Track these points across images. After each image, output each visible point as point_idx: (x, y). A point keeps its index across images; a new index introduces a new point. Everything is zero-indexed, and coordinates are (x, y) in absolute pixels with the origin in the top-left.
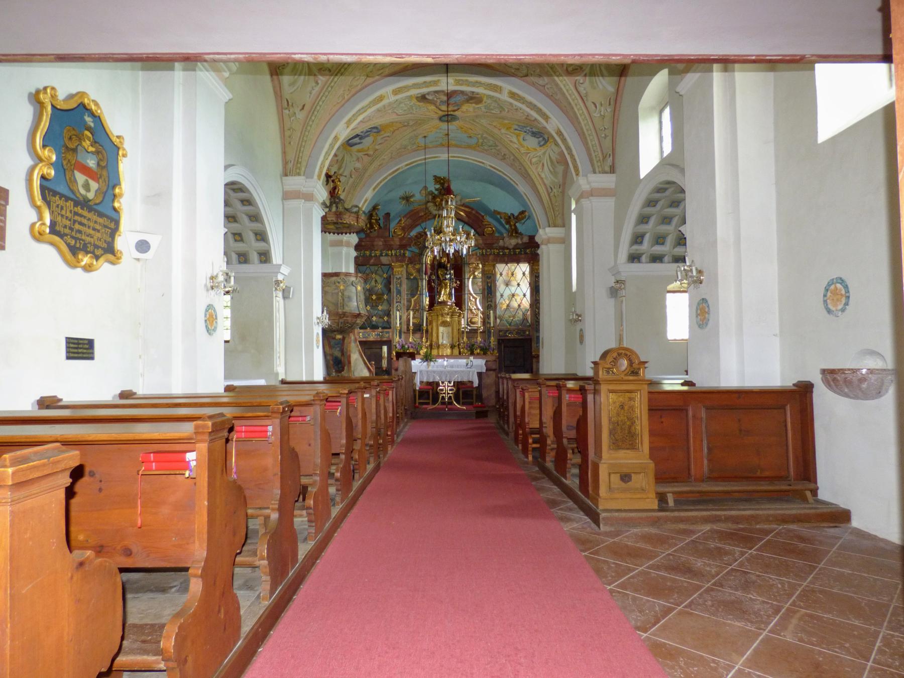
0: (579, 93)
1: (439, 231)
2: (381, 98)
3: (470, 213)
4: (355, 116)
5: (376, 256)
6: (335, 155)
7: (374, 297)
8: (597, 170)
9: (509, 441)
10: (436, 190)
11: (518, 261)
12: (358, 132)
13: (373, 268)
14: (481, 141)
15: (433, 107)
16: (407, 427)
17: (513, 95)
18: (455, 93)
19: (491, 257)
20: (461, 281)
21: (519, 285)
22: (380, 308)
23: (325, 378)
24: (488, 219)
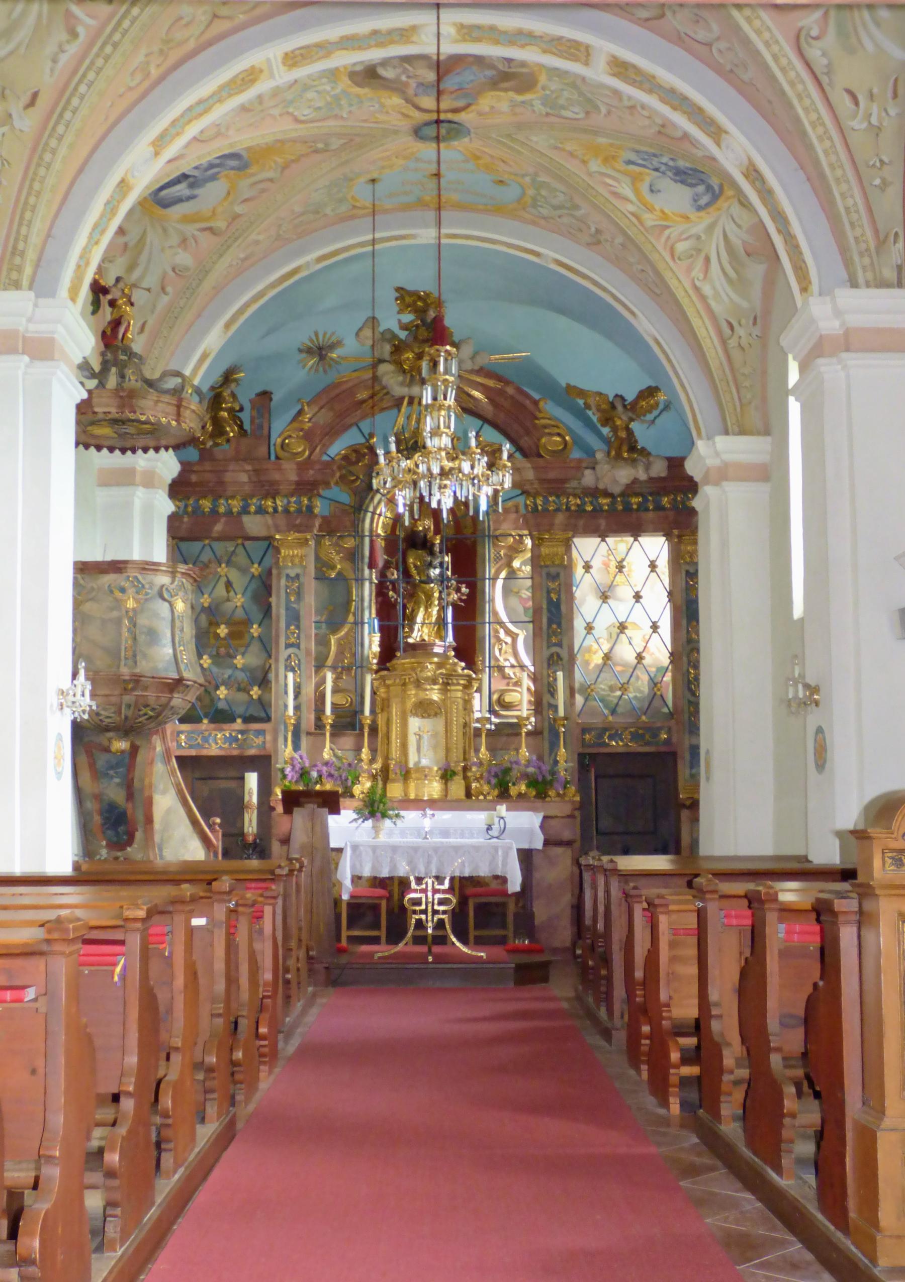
0: (808, 65)
1: (412, 445)
2: (251, 76)
3: (501, 392)
4: (178, 125)
5: (229, 513)
6: (121, 231)
7: (223, 631)
8: (861, 280)
9: (611, 1055)
10: (404, 327)
11: (636, 530)
12: (185, 167)
13: (220, 547)
14: (531, 192)
15: (396, 100)
16: (314, 1011)
17: (620, 68)
18: (458, 60)
19: (560, 518)
20: (472, 586)
21: (638, 597)
22: (239, 661)
23: (76, 867)
24: (551, 409)
